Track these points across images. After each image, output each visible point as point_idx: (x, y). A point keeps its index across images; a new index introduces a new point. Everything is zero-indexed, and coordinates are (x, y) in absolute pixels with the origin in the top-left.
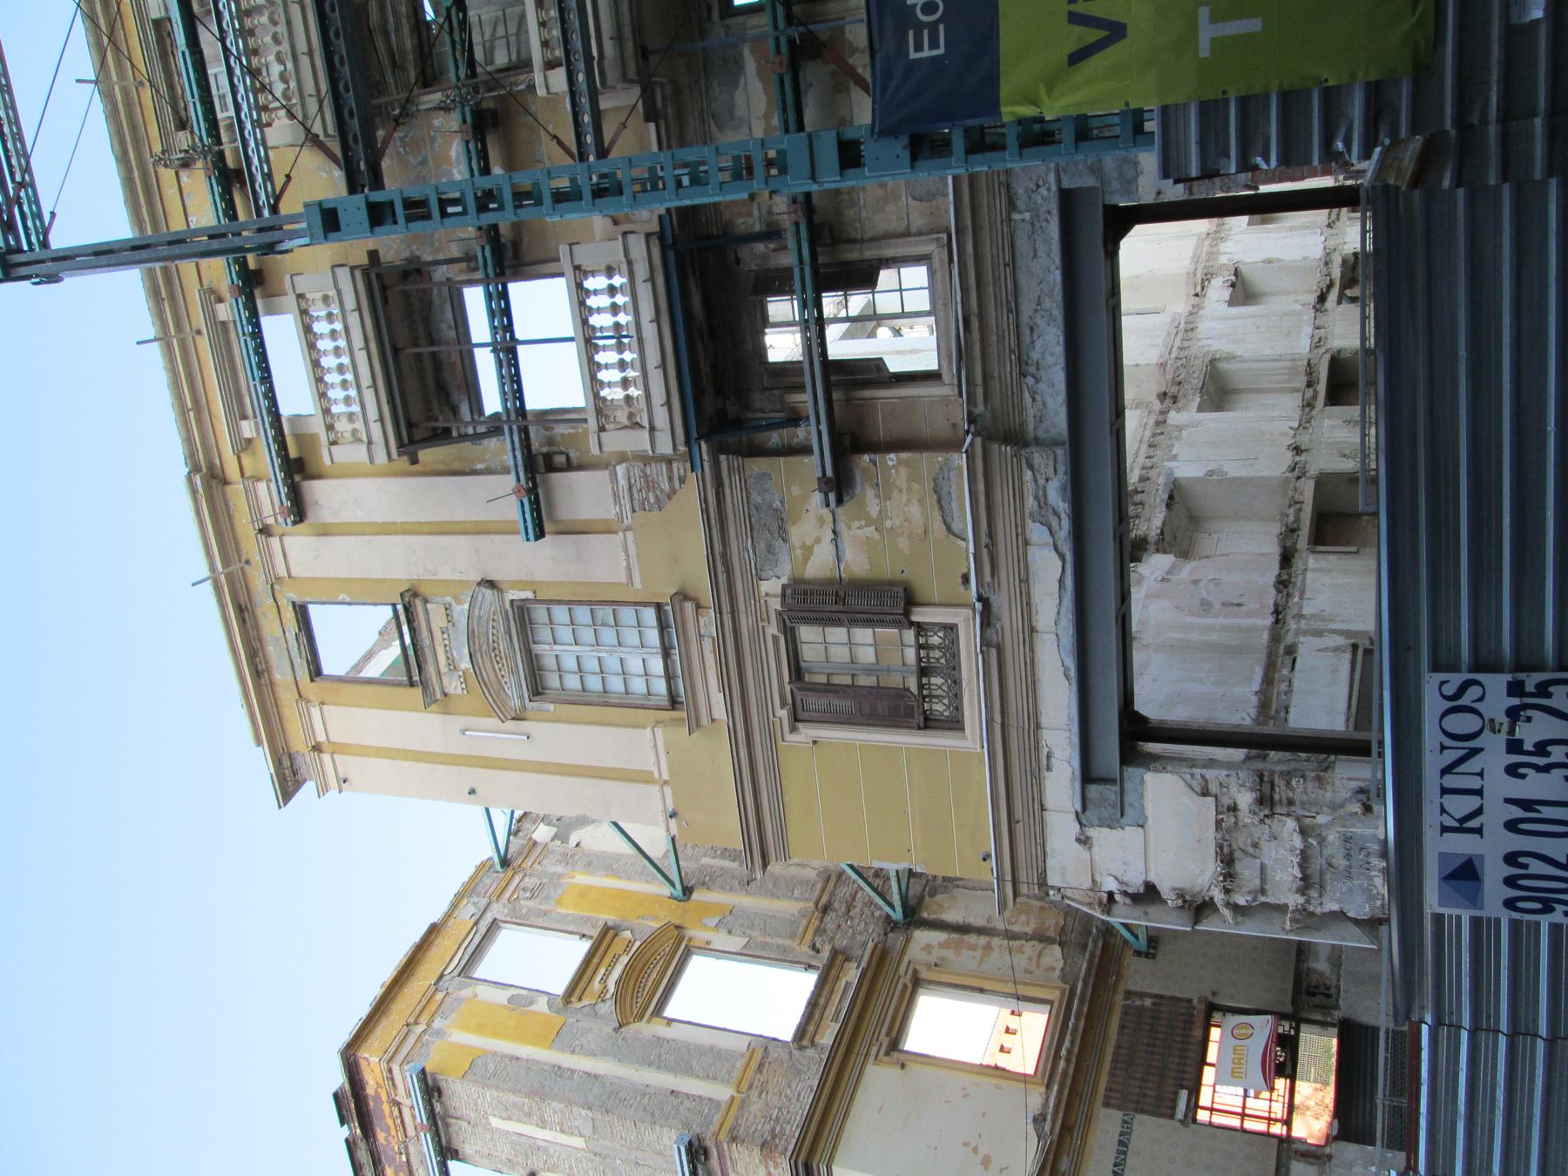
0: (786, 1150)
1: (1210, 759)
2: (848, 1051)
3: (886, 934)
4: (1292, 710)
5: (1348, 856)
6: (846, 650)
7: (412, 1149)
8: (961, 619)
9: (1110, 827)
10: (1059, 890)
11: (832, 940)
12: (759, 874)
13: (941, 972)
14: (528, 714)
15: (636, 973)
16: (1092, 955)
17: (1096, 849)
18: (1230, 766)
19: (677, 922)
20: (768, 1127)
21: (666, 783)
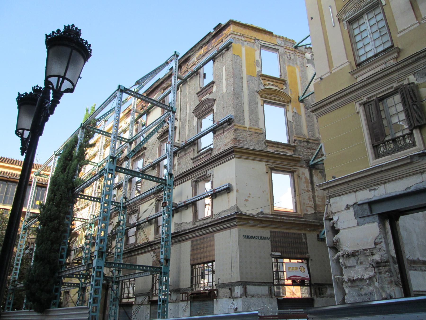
0: (236, 145)
1: (389, 245)
2: (267, 156)
3: (304, 161)
4: (415, 272)
5: (366, 294)
6: (395, 112)
7: (213, 50)
8: (419, 147)
9: (355, 215)
10: (330, 203)
11: (299, 146)
12: (309, 110)
13: (297, 179)
14: (342, 23)
15: (274, 92)
16: (314, 222)
17: (346, 211)
18: (388, 251)
19: (292, 100)
20: (241, 139)
21: (331, 73)
